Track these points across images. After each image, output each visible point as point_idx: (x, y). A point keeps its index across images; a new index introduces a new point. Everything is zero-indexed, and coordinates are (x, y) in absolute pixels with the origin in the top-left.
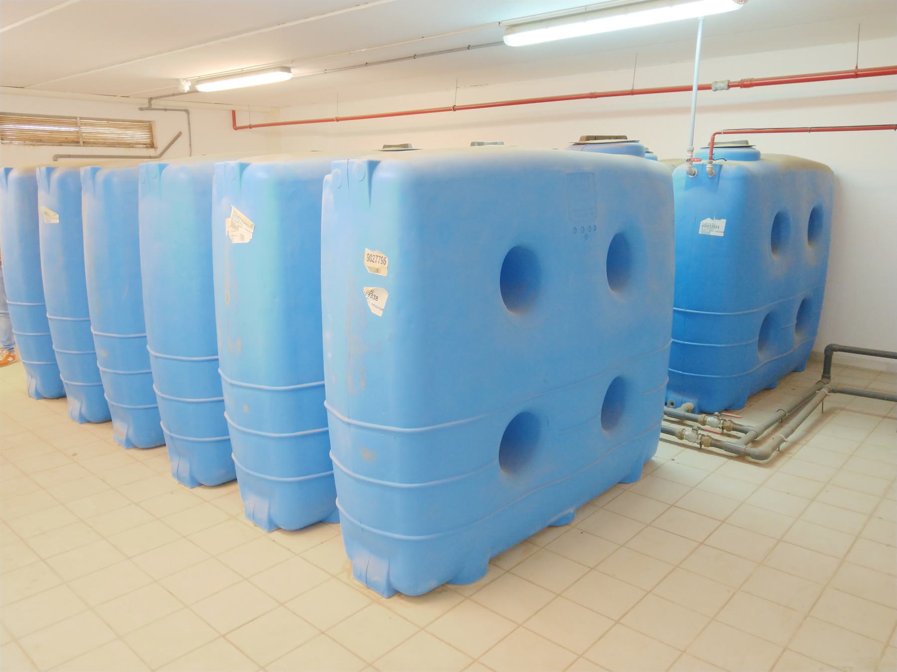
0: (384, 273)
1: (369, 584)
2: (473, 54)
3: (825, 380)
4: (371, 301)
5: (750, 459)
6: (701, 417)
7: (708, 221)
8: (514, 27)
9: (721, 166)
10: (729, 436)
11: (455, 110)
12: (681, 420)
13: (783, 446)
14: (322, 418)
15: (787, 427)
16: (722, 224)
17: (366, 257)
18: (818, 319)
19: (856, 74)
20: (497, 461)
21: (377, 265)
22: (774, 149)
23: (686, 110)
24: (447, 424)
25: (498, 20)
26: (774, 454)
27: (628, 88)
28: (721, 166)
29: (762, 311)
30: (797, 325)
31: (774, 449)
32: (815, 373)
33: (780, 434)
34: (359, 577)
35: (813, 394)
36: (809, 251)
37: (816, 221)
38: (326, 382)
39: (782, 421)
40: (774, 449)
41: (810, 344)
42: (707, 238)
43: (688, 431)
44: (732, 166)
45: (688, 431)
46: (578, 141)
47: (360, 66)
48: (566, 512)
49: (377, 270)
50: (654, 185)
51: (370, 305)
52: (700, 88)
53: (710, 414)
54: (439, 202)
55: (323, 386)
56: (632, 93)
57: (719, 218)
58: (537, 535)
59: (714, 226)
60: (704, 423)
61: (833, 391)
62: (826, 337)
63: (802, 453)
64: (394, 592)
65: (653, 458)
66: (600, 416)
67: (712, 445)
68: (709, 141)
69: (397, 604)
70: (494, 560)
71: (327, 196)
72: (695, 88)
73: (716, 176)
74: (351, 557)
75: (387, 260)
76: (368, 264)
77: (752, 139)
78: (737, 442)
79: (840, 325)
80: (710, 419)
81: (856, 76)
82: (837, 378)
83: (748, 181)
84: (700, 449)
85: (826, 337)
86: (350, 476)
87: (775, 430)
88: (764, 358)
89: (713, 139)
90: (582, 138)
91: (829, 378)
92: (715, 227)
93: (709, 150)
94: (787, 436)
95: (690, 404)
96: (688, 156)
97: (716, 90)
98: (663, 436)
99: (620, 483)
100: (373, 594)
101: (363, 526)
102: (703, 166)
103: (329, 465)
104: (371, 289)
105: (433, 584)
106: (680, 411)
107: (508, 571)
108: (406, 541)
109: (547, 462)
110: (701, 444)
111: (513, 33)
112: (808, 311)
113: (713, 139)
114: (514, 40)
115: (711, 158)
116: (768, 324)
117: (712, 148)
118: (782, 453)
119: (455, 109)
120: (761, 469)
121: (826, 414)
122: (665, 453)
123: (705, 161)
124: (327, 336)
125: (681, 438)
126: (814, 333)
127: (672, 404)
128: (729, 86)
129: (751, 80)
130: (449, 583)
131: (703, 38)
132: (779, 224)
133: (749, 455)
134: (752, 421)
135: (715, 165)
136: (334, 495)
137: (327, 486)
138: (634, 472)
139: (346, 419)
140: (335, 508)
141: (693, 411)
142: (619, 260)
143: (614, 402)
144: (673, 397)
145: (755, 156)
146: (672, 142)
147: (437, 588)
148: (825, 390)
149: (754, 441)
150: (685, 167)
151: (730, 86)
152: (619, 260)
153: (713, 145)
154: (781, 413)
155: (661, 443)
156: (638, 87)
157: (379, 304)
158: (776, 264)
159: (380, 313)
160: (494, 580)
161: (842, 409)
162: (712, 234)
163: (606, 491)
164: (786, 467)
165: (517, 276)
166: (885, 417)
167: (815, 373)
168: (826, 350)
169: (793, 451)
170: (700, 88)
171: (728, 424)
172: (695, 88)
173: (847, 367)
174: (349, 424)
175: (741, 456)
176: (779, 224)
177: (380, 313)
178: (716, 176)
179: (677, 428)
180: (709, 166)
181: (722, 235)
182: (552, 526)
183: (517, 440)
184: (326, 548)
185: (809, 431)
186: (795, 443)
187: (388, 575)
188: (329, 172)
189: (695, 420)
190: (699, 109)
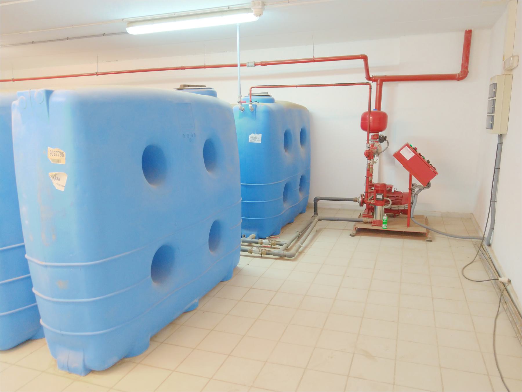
0: (63, 162)
1: (70, 370)
2: (106, 39)
3: (315, 215)
4: (55, 182)
5: (286, 258)
6: (260, 241)
7: (253, 135)
8: (132, 23)
9: (256, 106)
10: (275, 248)
11: (98, 75)
12: (250, 243)
13: (301, 249)
14: (25, 267)
15: (301, 240)
16: (260, 136)
17: (49, 153)
18: (309, 183)
19: (314, 61)
20: (150, 277)
21: (57, 158)
22: (282, 97)
23: (234, 78)
24: (116, 257)
25: (122, 17)
26: (297, 254)
27: (202, 64)
28: (256, 106)
29: (282, 182)
30: (300, 189)
31: (297, 252)
32: (310, 213)
33: (299, 243)
34: (62, 367)
35: (311, 222)
36: (302, 150)
37: (303, 134)
38: (26, 243)
39: (298, 237)
40: (297, 252)
41: (306, 199)
42: (253, 144)
43: (254, 249)
44: (262, 106)
45: (254, 249)
46: (179, 87)
47: (29, 43)
48: (194, 302)
49: (58, 161)
50: (223, 112)
51: (54, 184)
52: (242, 65)
53: (264, 239)
54: (95, 118)
55: (23, 246)
56: (205, 67)
57: (258, 134)
58: (179, 318)
59: (256, 138)
60: (262, 243)
61: (320, 220)
62: (313, 195)
63: (309, 251)
64: (89, 371)
65: (238, 266)
66: (208, 243)
67: (267, 254)
68: (249, 92)
69: (92, 378)
70: (153, 338)
71: (16, 115)
72: (239, 65)
73: (254, 111)
74: (55, 355)
75: (65, 153)
76: (50, 157)
77: (269, 91)
78: (280, 250)
79: (319, 187)
80: (264, 241)
81: (314, 61)
82: (321, 214)
83: (269, 113)
84: (261, 257)
85: (313, 195)
86: (49, 301)
87: (296, 243)
88: (286, 207)
89: (251, 91)
90: (181, 86)
91: (317, 214)
92: (256, 138)
93: (249, 97)
94: (302, 244)
95: (253, 235)
96: (239, 100)
97: (249, 67)
98: (242, 253)
99: (221, 281)
100: (74, 376)
101: (63, 332)
102: (247, 105)
103: (33, 298)
104: (54, 173)
105: (115, 359)
106: (249, 239)
107: (162, 343)
108: (94, 335)
109: (180, 275)
110: (261, 254)
111: (132, 26)
112: (304, 182)
113: (251, 91)
114: (132, 31)
115: (251, 101)
116: (287, 188)
117: (251, 96)
118: (300, 253)
119: (97, 74)
120: (292, 262)
121: (318, 232)
122: (244, 262)
123: (248, 103)
124: (24, 210)
125: (251, 253)
126: (308, 193)
127: (244, 236)
128: (255, 65)
129: (266, 62)
130: (126, 357)
131: (240, 37)
132: (287, 136)
133: (285, 256)
134: (285, 239)
135: (253, 105)
136: (38, 317)
137: (34, 313)
138: (228, 275)
139: (44, 263)
140: (41, 327)
141: (255, 238)
142: (210, 154)
143: (215, 234)
144: (245, 232)
145: (272, 101)
146: (230, 93)
147: (118, 362)
148: (316, 220)
149: (286, 249)
150: (238, 106)
151: (256, 65)
152: (210, 154)
153: (251, 95)
154: (298, 233)
155: (241, 257)
156: (207, 64)
157: (61, 183)
158: (287, 157)
159: (62, 189)
160: (154, 349)
161: (325, 228)
162: (256, 142)
163: (214, 288)
164: (303, 259)
165: (152, 163)
166: (343, 230)
167: (310, 213)
168: (314, 201)
169: (305, 251)
170: (242, 65)
171: (273, 242)
172: (239, 65)
173: (324, 209)
174: (46, 266)
175: (282, 257)
176: (287, 136)
177: (62, 189)
178: (254, 111)
179: (248, 248)
180: (250, 105)
181: (260, 142)
182: (186, 312)
183: (161, 263)
184: (37, 355)
185: (312, 240)
186: (306, 247)
187: (84, 361)
188: (16, 99)
189: (257, 243)
190: (241, 78)
